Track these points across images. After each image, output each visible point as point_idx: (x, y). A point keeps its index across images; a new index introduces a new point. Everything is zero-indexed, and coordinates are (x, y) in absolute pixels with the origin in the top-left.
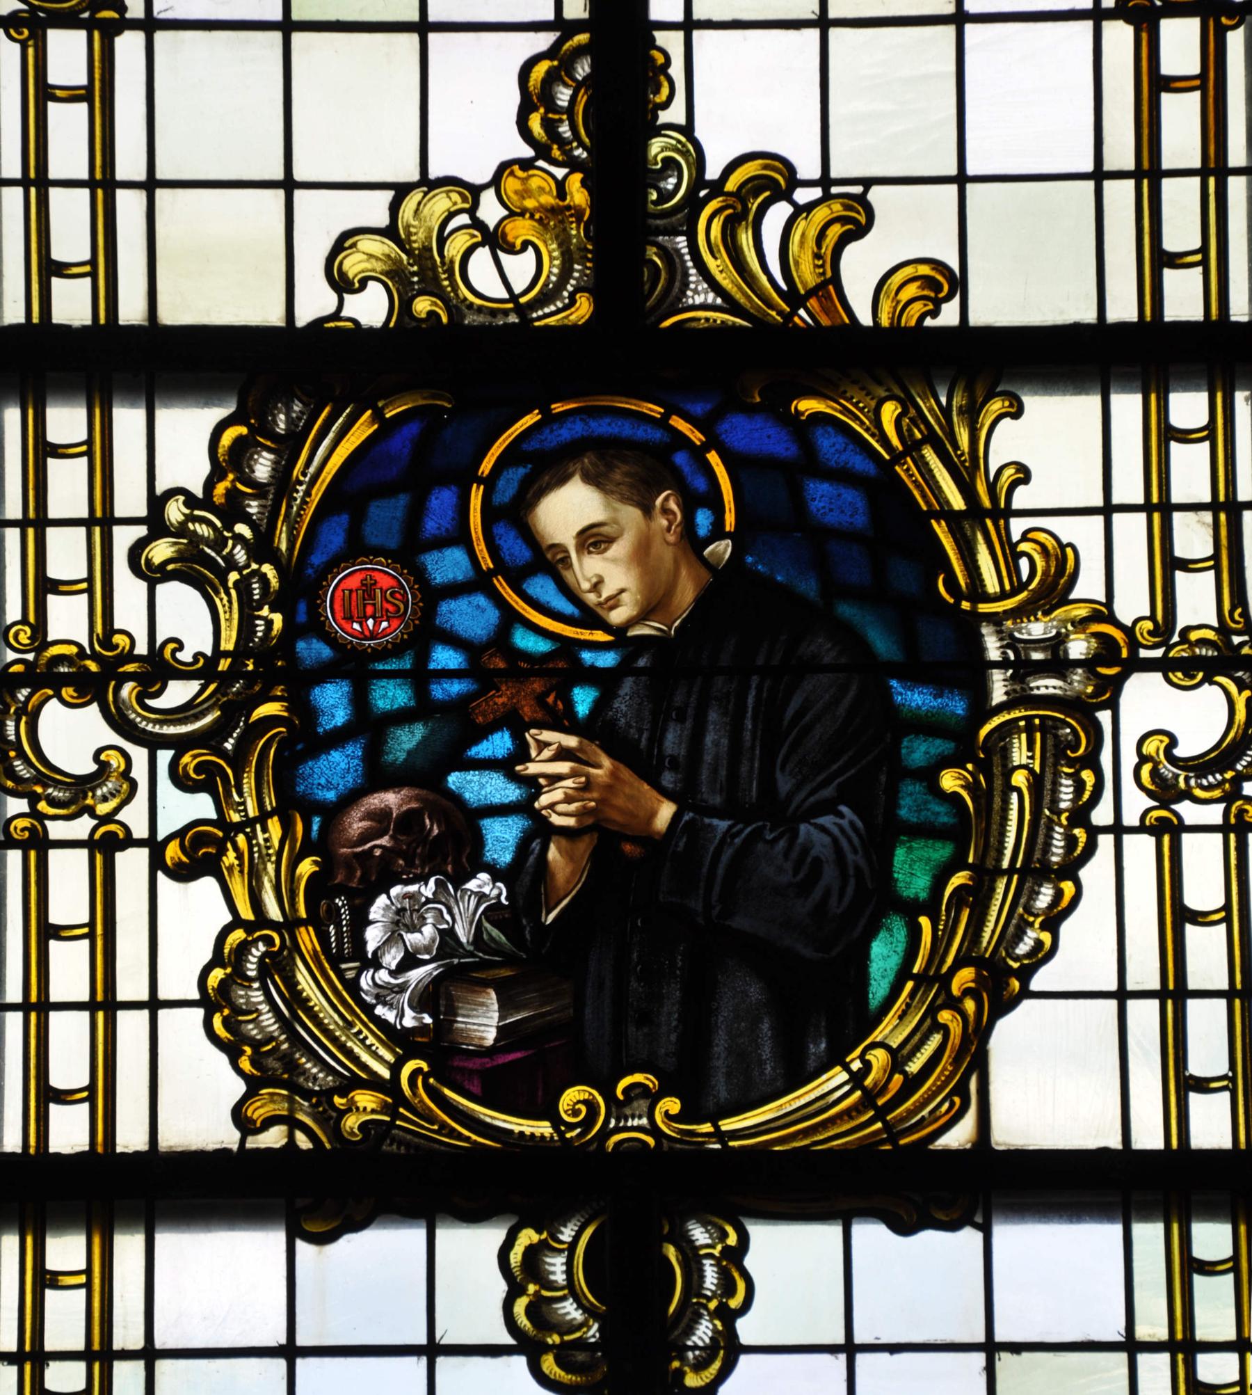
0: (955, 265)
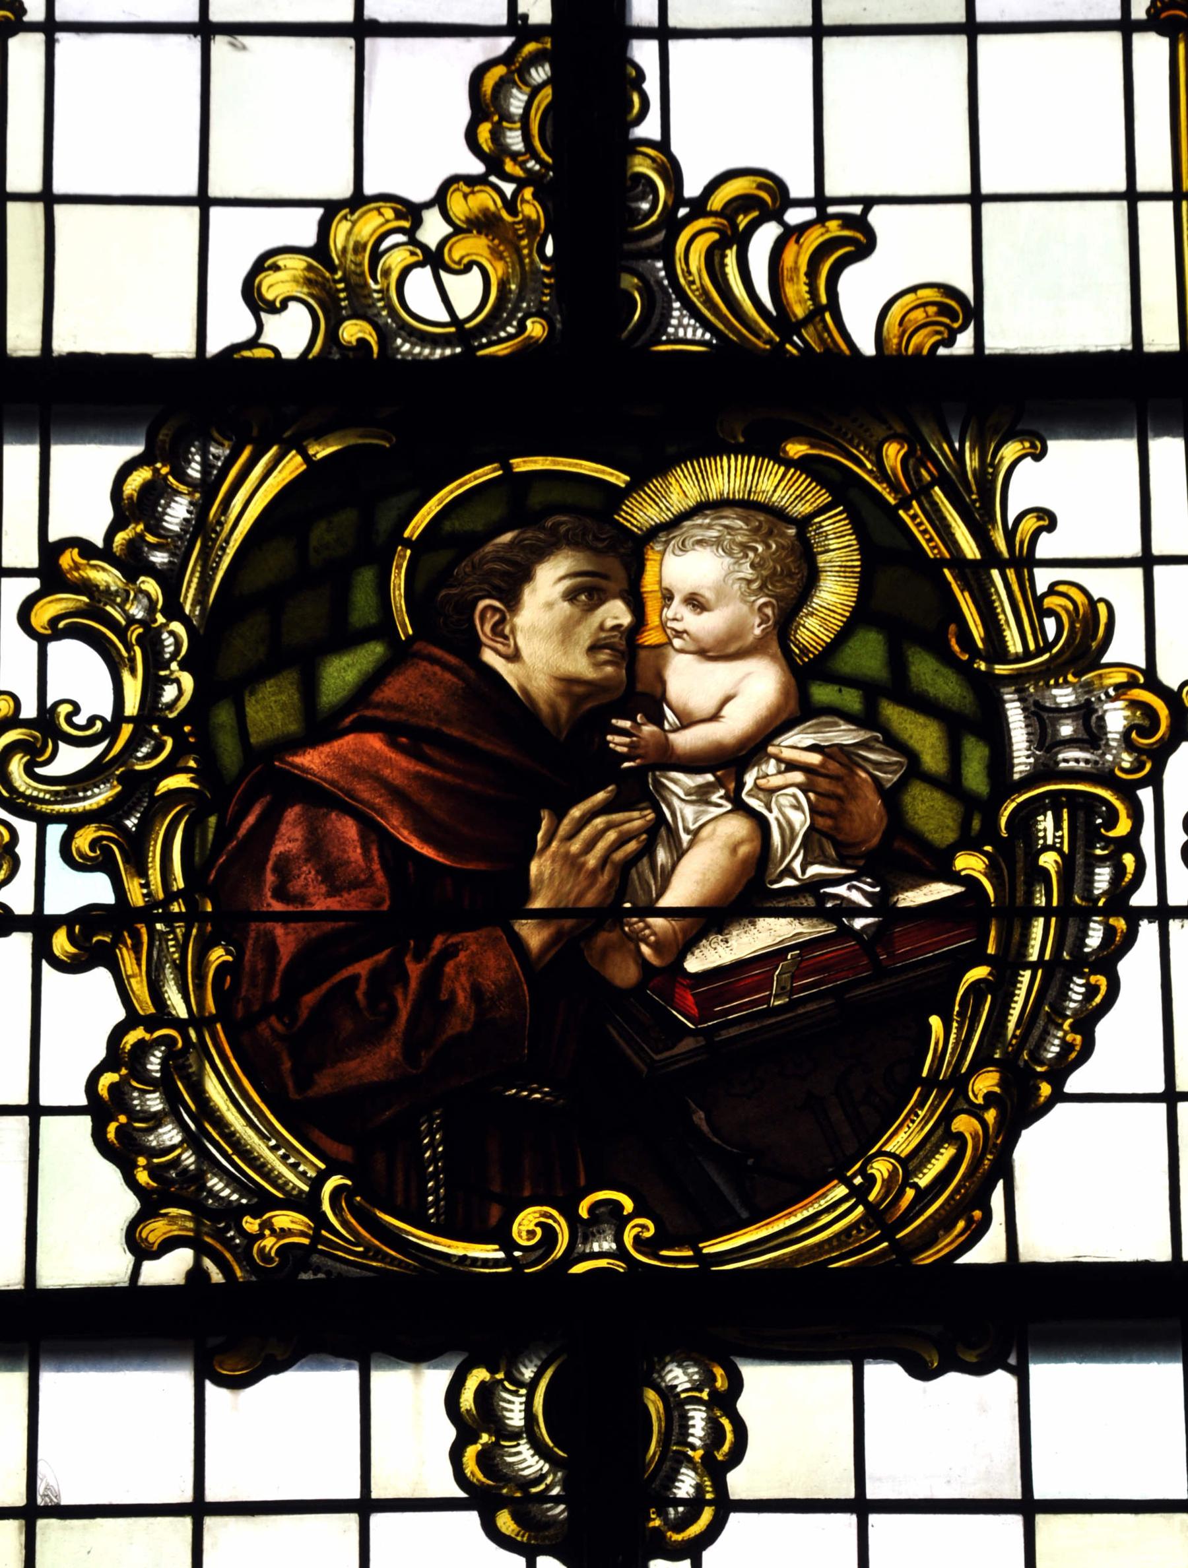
0: (968, 289)
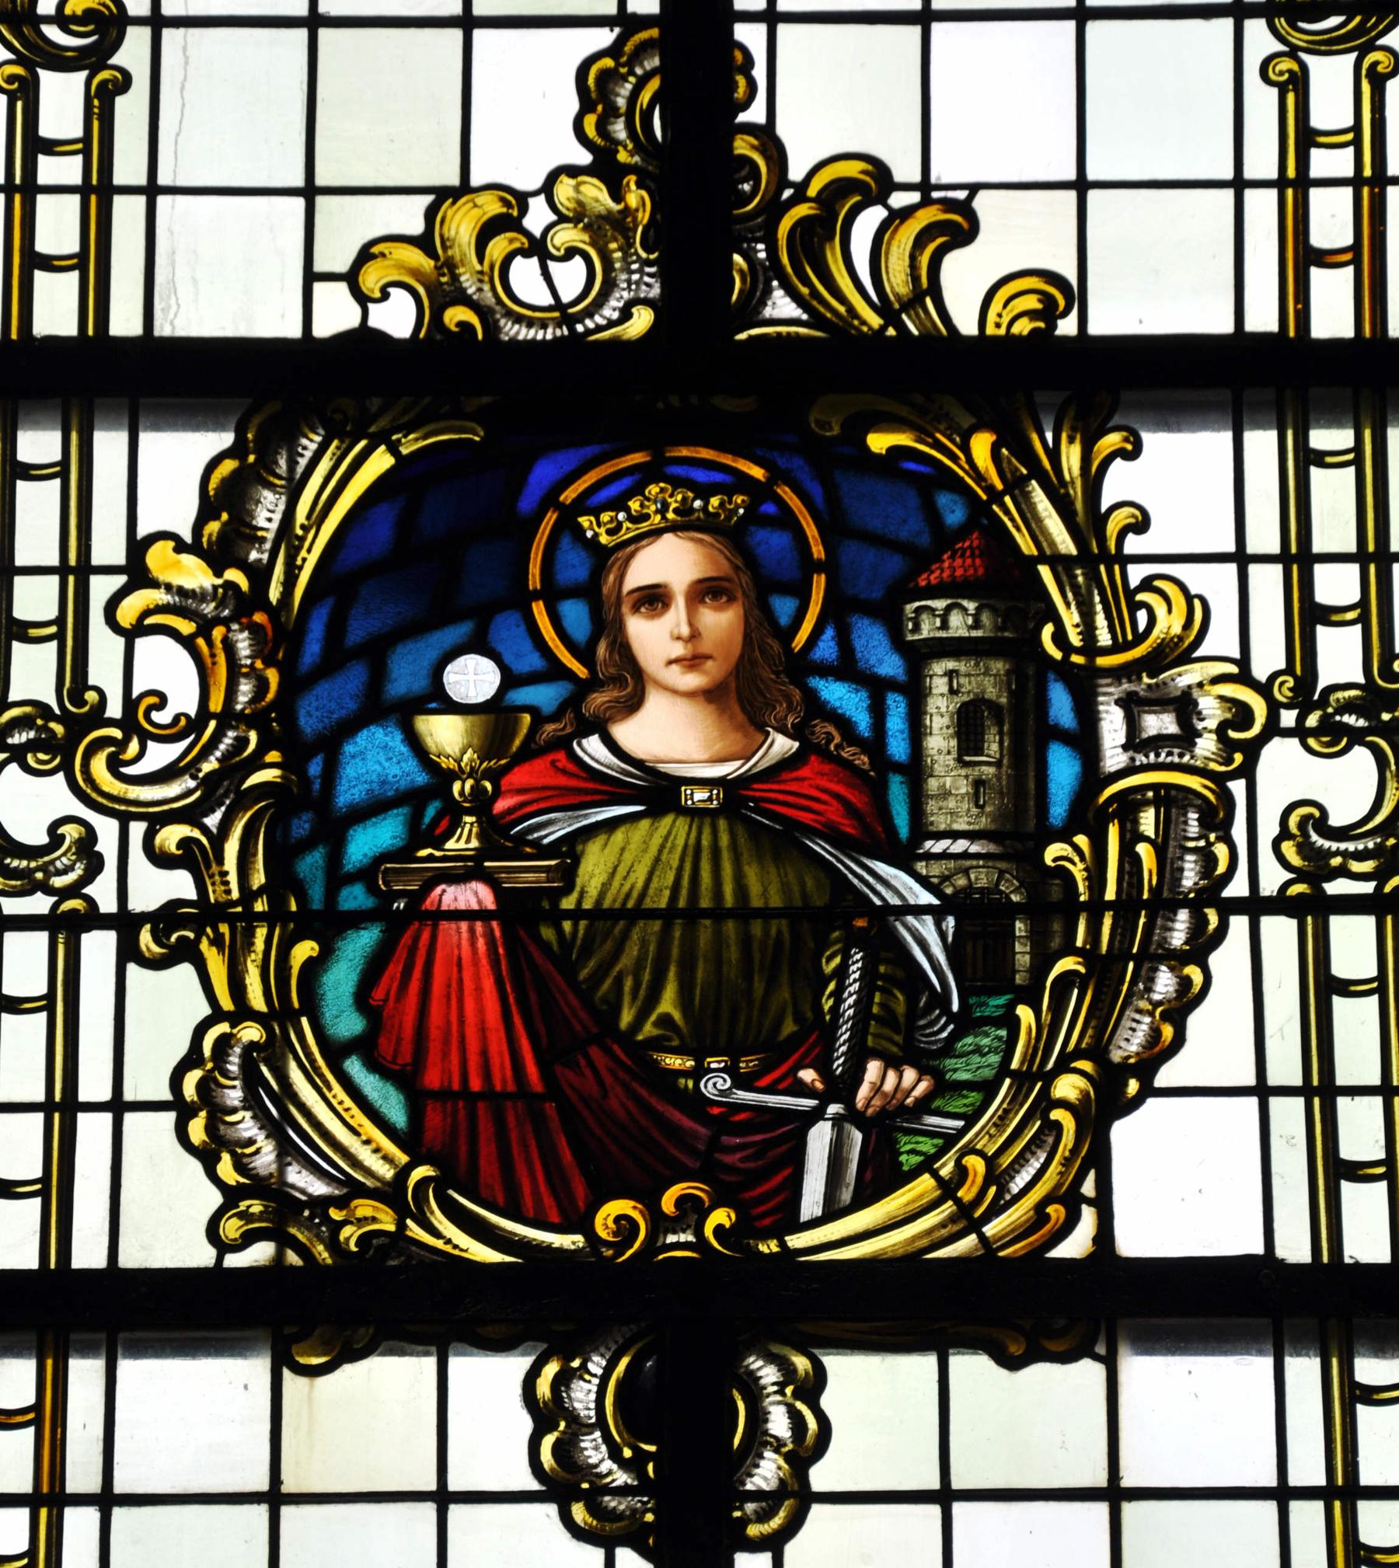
0: (1073, 278)
